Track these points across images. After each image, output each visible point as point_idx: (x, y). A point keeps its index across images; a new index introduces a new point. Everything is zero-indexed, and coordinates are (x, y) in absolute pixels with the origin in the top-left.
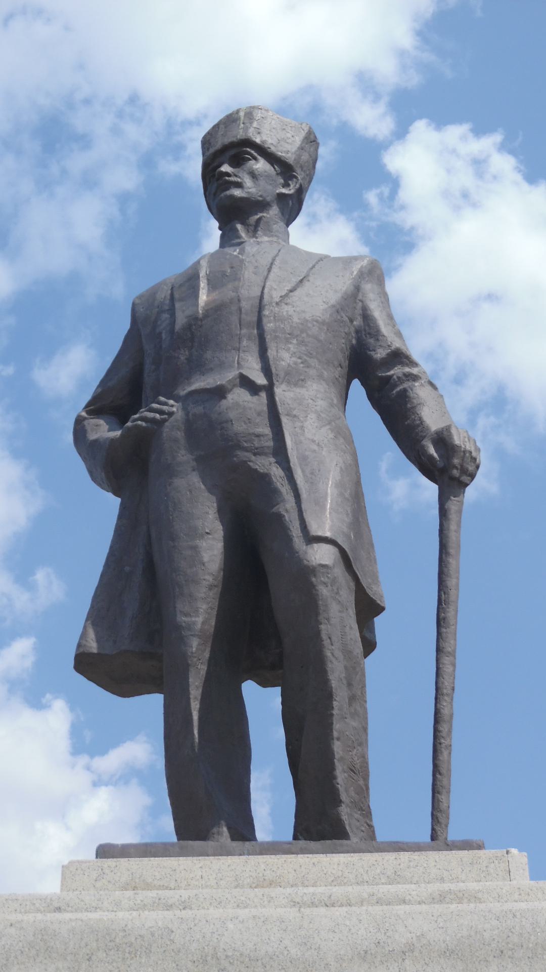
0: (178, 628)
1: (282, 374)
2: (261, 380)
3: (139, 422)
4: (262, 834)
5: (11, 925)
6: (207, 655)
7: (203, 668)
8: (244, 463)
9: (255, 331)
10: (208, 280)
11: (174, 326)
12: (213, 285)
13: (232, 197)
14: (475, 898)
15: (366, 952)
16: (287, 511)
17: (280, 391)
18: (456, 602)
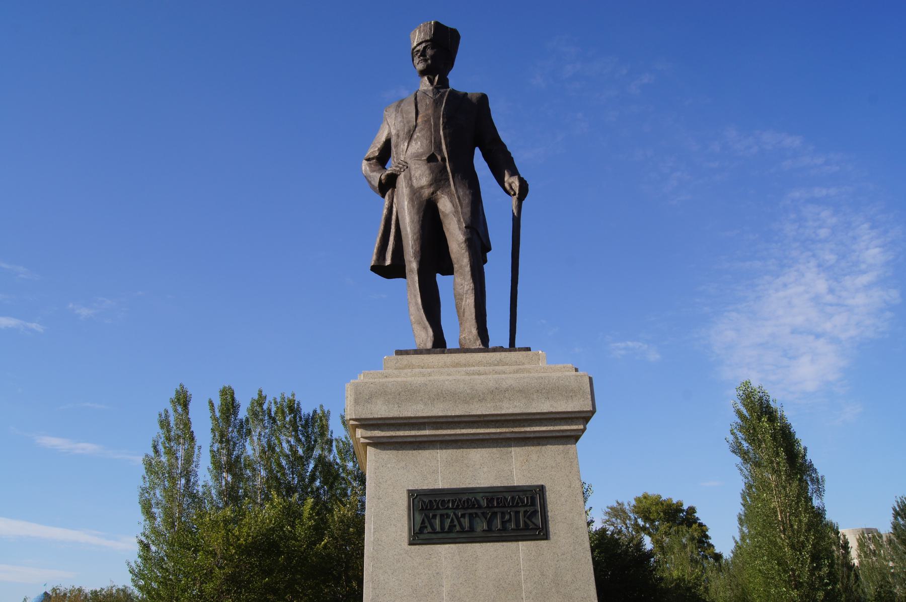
4: (449, 345)
14: (529, 371)
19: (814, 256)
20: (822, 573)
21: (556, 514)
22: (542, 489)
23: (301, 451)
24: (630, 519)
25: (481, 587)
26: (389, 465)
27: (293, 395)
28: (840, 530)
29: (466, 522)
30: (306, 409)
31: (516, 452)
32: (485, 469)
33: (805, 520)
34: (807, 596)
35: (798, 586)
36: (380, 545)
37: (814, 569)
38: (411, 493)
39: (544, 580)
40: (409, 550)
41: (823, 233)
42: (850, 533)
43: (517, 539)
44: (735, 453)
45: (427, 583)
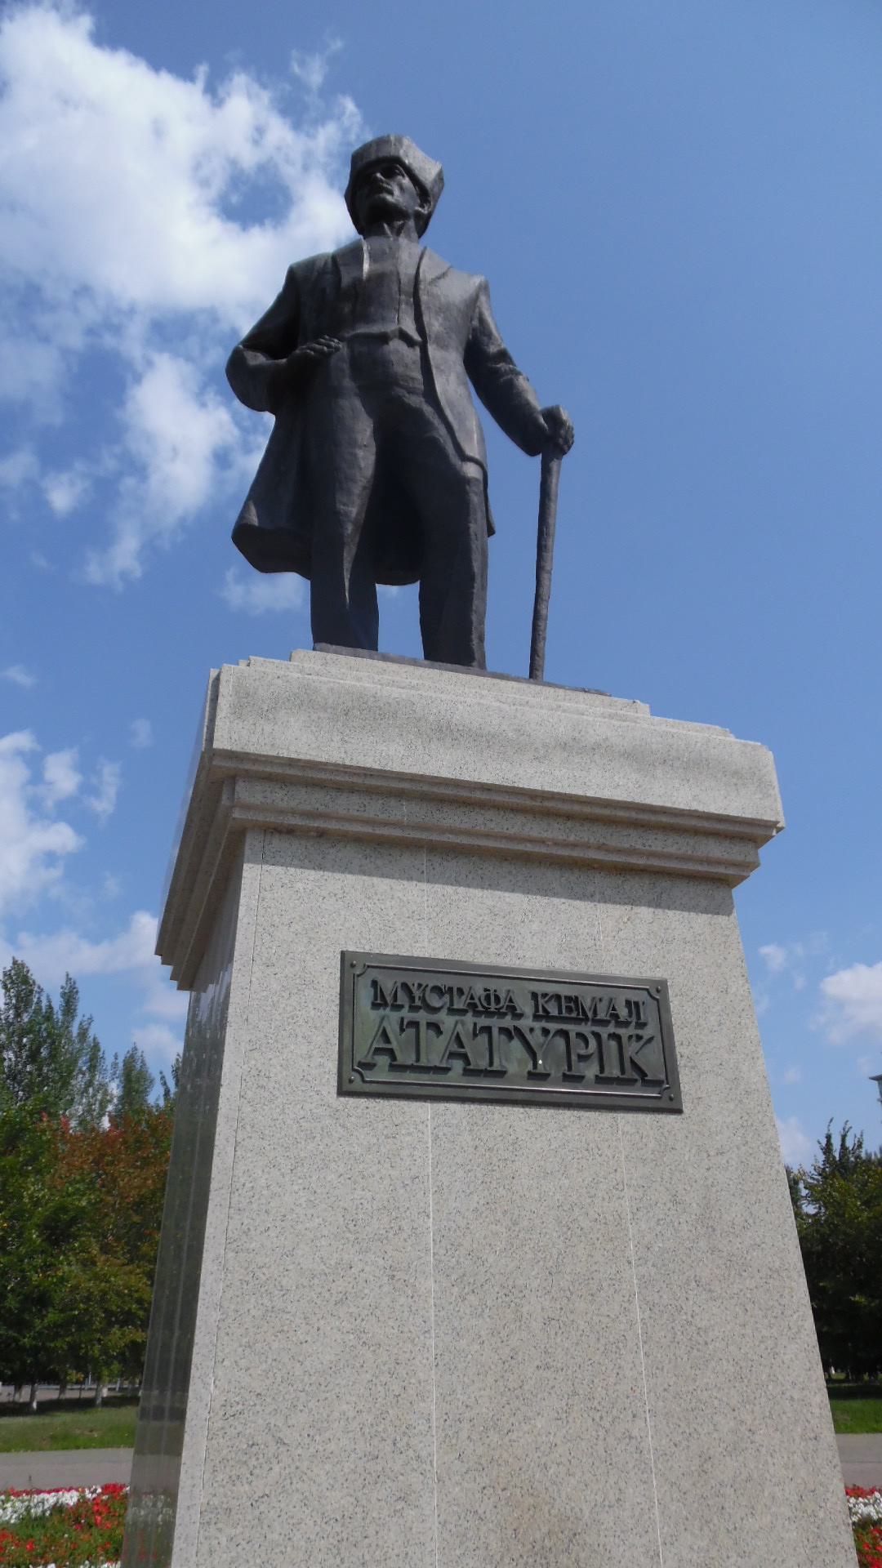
0: (337, 513)
1: (433, 336)
2: (417, 337)
3: (308, 351)
5: (279, 677)
6: (357, 539)
7: (354, 549)
8: (400, 398)
9: (412, 300)
10: (370, 253)
11: (340, 280)
12: (374, 258)
13: (384, 200)
15: (566, 744)
16: (440, 436)
17: (432, 350)
18: (553, 536)
21: (700, 1051)
25: (526, 1223)
26: (299, 886)
32: (535, 927)
36: (263, 1087)
39: (678, 1217)
40: (340, 1108)
45: (386, 1203)
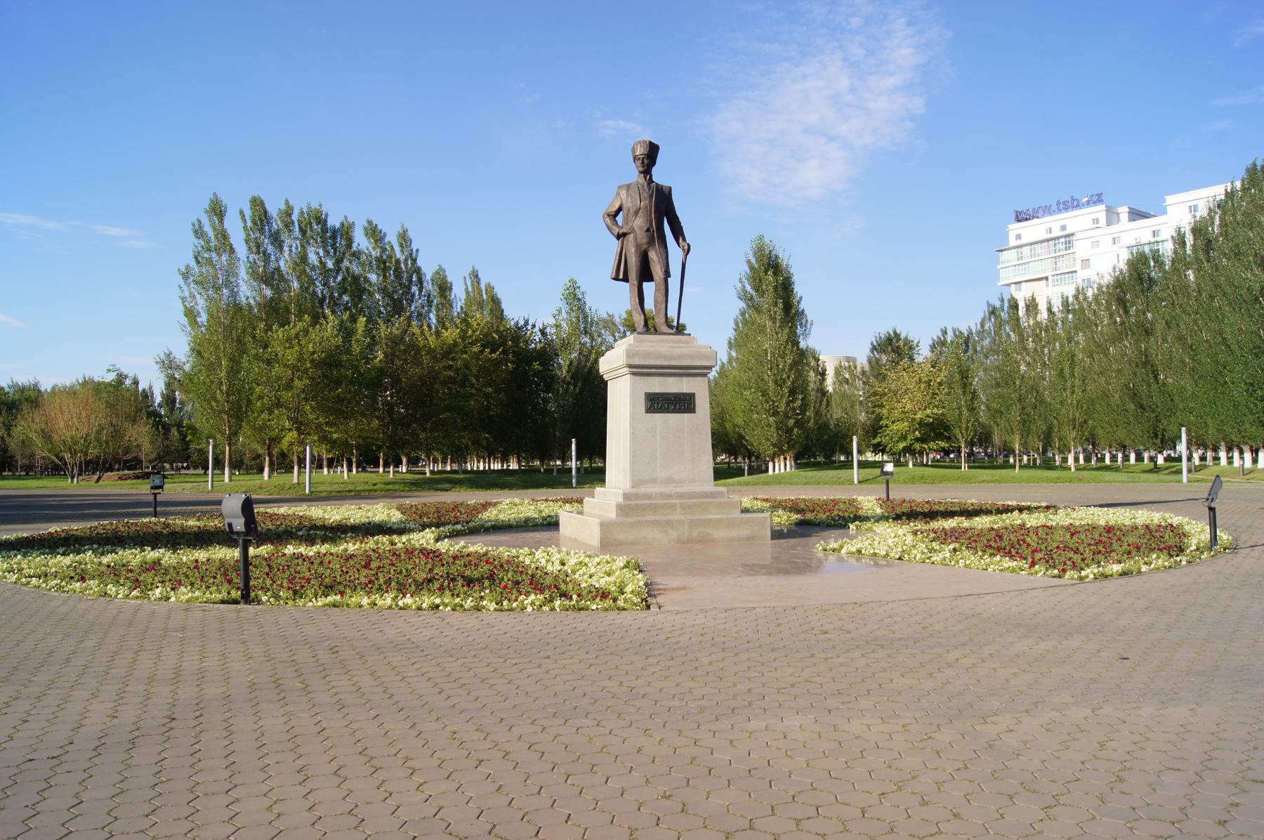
19: (841, 47)
20: (795, 405)
22: (694, 394)
23: (330, 264)
24: (619, 332)
27: (321, 205)
28: (820, 357)
29: (666, 406)
30: (334, 221)
31: (685, 379)
33: (789, 361)
34: (781, 422)
35: (775, 414)
37: (790, 401)
38: (646, 393)
41: (856, 22)
42: (829, 363)
43: (684, 413)
44: (741, 299)
